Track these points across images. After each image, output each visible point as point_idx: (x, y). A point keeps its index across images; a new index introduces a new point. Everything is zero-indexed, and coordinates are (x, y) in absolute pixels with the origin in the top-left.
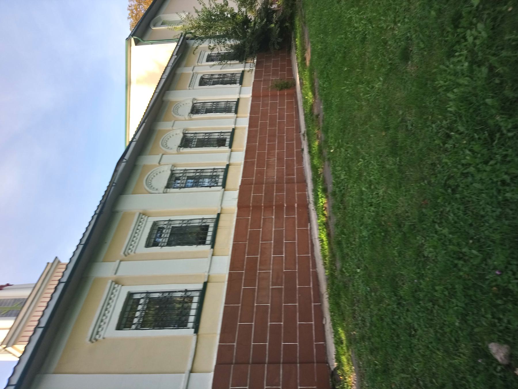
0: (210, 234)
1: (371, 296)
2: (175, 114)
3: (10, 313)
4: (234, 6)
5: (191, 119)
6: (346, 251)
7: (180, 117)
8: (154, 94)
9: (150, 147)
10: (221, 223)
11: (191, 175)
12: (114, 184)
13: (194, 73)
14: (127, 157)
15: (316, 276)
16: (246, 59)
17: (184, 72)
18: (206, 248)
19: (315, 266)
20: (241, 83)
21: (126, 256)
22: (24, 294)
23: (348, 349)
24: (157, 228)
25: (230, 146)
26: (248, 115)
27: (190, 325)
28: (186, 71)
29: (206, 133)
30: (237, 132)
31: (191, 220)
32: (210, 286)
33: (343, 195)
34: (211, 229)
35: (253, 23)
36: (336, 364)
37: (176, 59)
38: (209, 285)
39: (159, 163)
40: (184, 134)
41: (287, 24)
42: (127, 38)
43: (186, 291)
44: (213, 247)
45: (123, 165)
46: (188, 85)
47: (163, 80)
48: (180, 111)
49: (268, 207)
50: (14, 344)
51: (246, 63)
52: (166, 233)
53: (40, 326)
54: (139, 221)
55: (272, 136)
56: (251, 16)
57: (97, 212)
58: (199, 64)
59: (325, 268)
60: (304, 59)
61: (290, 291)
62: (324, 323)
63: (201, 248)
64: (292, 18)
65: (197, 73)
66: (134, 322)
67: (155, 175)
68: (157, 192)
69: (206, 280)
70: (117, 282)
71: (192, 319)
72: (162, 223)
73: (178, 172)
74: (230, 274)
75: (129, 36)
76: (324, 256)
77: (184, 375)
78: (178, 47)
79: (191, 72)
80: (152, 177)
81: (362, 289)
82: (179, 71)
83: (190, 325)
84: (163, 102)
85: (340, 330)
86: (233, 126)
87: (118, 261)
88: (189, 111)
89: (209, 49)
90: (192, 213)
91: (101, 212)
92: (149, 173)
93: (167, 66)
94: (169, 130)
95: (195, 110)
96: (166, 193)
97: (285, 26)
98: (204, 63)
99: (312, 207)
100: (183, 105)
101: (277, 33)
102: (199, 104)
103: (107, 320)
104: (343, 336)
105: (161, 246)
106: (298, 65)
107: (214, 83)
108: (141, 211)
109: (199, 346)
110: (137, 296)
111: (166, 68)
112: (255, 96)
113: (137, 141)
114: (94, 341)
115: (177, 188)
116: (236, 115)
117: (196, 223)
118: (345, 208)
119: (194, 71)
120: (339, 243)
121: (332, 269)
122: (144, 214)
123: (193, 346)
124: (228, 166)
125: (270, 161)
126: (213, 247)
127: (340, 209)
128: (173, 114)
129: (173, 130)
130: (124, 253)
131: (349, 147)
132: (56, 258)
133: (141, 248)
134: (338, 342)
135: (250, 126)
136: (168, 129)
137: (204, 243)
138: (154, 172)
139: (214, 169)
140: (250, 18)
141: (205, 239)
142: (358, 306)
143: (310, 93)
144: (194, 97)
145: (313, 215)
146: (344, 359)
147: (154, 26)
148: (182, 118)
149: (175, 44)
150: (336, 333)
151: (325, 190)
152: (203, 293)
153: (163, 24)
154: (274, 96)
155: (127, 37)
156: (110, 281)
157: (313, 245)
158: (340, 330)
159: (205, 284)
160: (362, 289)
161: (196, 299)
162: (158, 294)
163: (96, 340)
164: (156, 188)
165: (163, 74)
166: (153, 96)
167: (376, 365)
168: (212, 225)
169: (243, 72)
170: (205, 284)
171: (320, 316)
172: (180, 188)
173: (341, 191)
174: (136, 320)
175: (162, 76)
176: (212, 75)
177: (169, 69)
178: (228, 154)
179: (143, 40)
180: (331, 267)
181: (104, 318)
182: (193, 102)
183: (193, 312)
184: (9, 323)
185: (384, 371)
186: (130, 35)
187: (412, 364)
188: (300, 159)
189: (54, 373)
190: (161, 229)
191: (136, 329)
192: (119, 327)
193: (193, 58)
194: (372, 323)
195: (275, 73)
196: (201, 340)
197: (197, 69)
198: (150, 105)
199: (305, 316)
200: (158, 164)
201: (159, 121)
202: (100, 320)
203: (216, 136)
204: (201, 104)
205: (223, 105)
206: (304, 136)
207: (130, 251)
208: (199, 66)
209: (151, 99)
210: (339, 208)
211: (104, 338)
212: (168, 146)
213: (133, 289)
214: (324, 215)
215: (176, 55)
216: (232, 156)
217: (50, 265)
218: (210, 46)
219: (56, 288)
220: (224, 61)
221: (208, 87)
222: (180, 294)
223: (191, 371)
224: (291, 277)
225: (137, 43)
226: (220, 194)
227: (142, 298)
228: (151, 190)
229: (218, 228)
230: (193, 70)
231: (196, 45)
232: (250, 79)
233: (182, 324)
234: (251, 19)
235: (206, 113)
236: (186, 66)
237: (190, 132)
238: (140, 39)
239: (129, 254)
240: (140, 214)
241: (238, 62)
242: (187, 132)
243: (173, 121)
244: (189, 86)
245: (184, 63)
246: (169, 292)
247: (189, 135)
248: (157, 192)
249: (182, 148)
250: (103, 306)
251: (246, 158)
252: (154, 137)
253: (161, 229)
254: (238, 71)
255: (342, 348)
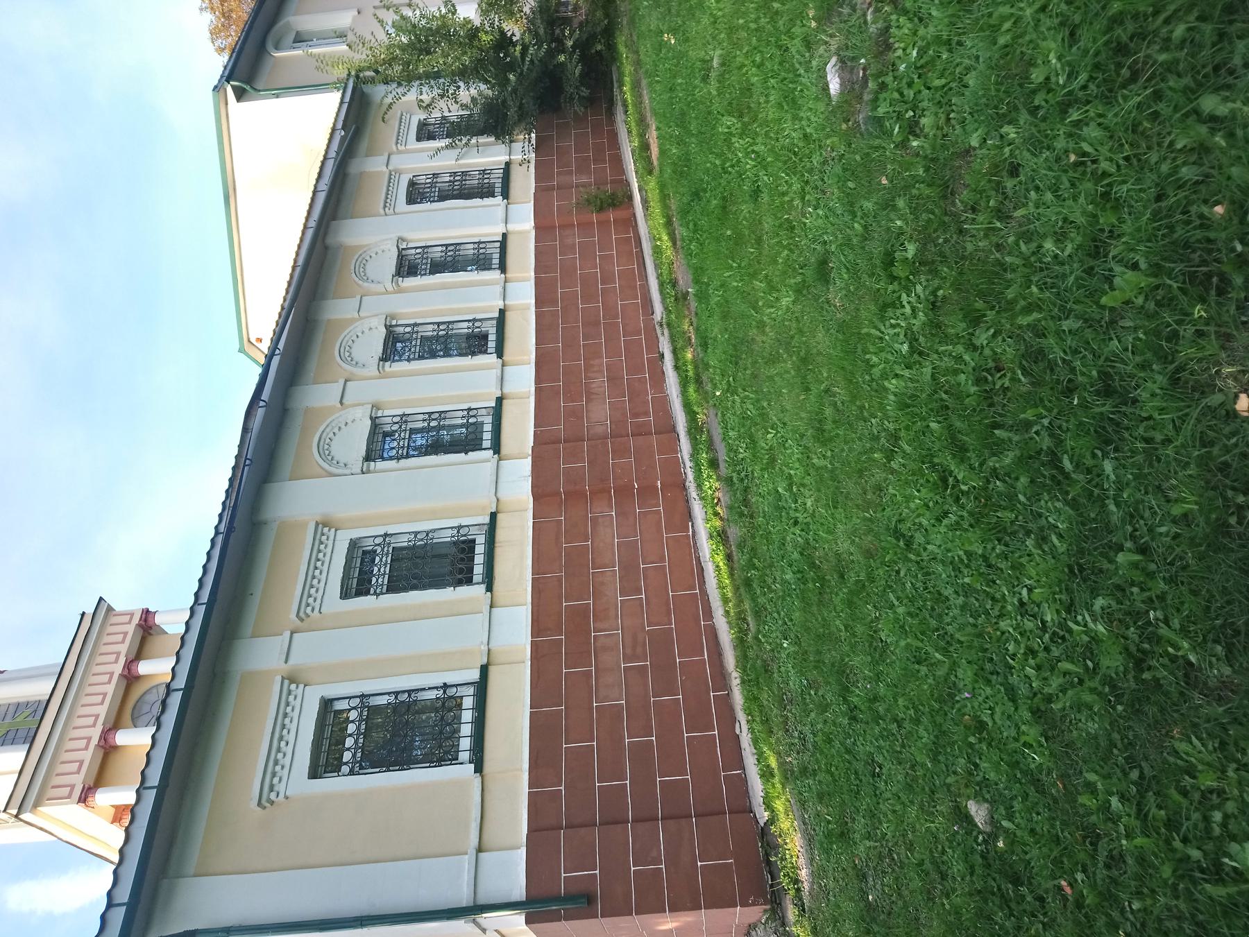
0: (479, 559)
1: (810, 694)
2: (361, 279)
3: (11, 735)
4: (468, 11)
5: (400, 291)
6: (762, 600)
7: (372, 286)
8: (303, 233)
9: (313, 365)
10: (501, 535)
11: (420, 425)
12: (248, 462)
13: (390, 172)
14: (265, 395)
15: (713, 633)
16: (510, 134)
17: (367, 170)
18: (476, 591)
19: (709, 614)
20: (506, 194)
21: (302, 620)
22: (41, 689)
23: (784, 787)
24: (360, 554)
25: (500, 353)
26: (533, 274)
27: (464, 756)
28: (373, 165)
29: (439, 324)
30: (508, 315)
31: (434, 531)
32: (493, 672)
33: (746, 490)
34: (480, 549)
35: (518, 48)
36: (766, 814)
37: (343, 139)
38: (493, 671)
39: (341, 403)
40: (389, 328)
41: (599, 47)
42: (216, 87)
43: (445, 686)
44: (490, 588)
45: (260, 413)
46: (382, 205)
47: (321, 197)
48: (371, 270)
49: (600, 491)
50: (37, 804)
51: (511, 142)
52: (381, 570)
53: (147, 785)
54: (318, 541)
55: (592, 324)
56: (514, 29)
57: (222, 528)
58: (401, 148)
59: (731, 628)
60: (645, 147)
61: (663, 667)
62: (738, 731)
63: (464, 591)
64: (609, 33)
65: (399, 172)
66: (345, 760)
67: (336, 430)
68: (347, 471)
69: (485, 661)
70: (292, 679)
71: (465, 744)
72: (370, 542)
73: (389, 420)
74: (535, 646)
75: (219, 81)
76: (725, 600)
77: (467, 857)
78: (345, 106)
79: (384, 168)
80: (331, 435)
81: (794, 683)
82: (354, 167)
83: (464, 756)
84: (326, 248)
85: (768, 752)
86: (500, 304)
87: (287, 634)
88: (393, 270)
89: (420, 107)
90: (434, 515)
91: (230, 529)
92: (321, 429)
93: (325, 158)
94: (353, 321)
95: (407, 267)
96: (369, 472)
97: (593, 51)
98: (413, 144)
99: (693, 493)
100: (376, 254)
101: (577, 74)
102: (413, 251)
103: (287, 761)
104: (773, 762)
105: (375, 593)
106: (633, 152)
107: (443, 197)
108: (318, 518)
109: (487, 797)
110: (341, 705)
111: (323, 163)
112: (542, 228)
113: (283, 355)
114: (268, 805)
115: (391, 458)
116: (503, 275)
117: (446, 537)
118: (752, 517)
119: (390, 167)
120: (748, 583)
121: (740, 630)
122: (325, 525)
123: (478, 798)
124: (500, 400)
125: (593, 386)
126: (490, 588)
127: (744, 515)
128: (357, 279)
129: (361, 318)
130: (298, 615)
131: (747, 397)
132: (101, 599)
133: (332, 601)
134: (767, 774)
135: (539, 302)
136: (349, 316)
137: (469, 581)
138: (335, 422)
139: (470, 409)
140: (509, 34)
141: (471, 570)
142: (791, 712)
143: (665, 238)
144: (399, 234)
145: (697, 509)
146: (779, 805)
147: (277, 48)
148: (380, 288)
149: (335, 97)
150: (760, 757)
151: (714, 464)
152: (481, 688)
153: (300, 39)
154: (585, 226)
155: (216, 82)
156: (279, 678)
157: (701, 570)
158: (768, 752)
159: (484, 670)
160: (794, 683)
161: (468, 702)
162: (387, 697)
163: (272, 803)
164: (342, 461)
165: (318, 180)
166: (302, 240)
167: (829, 822)
168: (481, 540)
169: (508, 164)
170: (484, 670)
171: (729, 718)
172: (399, 458)
173: (742, 480)
174: (347, 756)
175: (315, 187)
176: (435, 175)
177: (330, 164)
178: (496, 372)
179: (255, 89)
180: (739, 622)
181: (280, 756)
182: (398, 247)
183: (466, 730)
184: (13, 758)
185: (842, 834)
186: (222, 77)
187: (881, 823)
188: (658, 378)
189: (195, 876)
190: (368, 556)
191: (352, 773)
192: (314, 774)
193: (383, 132)
194: (815, 745)
195: (582, 168)
196: (490, 785)
197: (396, 162)
198: (301, 262)
199: (699, 719)
200: (339, 405)
201: (324, 297)
202: (273, 761)
203: (463, 328)
204: (418, 251)
205: (469, 251)
206: (661, 325)
207: (309, 609)
208: (399, 152)
209: (299, 247)
210: (741, 515)
211: (287, 798)
212: (355, 359)
213: (331, 691)
214: (716, 514)
215: (343, 128)
216: (506, 377)
217: (87, 620)
218: (422, 101)
219: (164, 703)
220: (460, 140)
221: (426, 206)
222: (432, 695)
223: (480, 850)
224: (661, 644)
225: (240, 95)
226: (490, 467)
227: (354, 708)
228: (332, 466)
229: (496, 545)
230: (387, 166)
231: (388, 100)
232: (525, 182)
233: (444, 755)
234: (513, 34)
235: (432, 273)
236: (370, 153)
237: (400, 322)
238: (248, 88)
239: (308, 616)
240: (317, 524)
241: (492, 139)
242: (394, 323)
243: (358, 297)
244: (385, 207)
245: (364, 145)
246: (409, 692)
247: (401, 330)
248: (347, 471)
249: (388, 364)
250: (273, 733)
251: (538, 380)
252: (319, 338)
253: (368, 556)
254: (494, 163)
255: (773, 785)
